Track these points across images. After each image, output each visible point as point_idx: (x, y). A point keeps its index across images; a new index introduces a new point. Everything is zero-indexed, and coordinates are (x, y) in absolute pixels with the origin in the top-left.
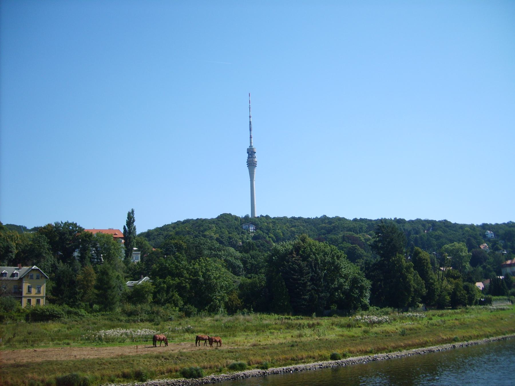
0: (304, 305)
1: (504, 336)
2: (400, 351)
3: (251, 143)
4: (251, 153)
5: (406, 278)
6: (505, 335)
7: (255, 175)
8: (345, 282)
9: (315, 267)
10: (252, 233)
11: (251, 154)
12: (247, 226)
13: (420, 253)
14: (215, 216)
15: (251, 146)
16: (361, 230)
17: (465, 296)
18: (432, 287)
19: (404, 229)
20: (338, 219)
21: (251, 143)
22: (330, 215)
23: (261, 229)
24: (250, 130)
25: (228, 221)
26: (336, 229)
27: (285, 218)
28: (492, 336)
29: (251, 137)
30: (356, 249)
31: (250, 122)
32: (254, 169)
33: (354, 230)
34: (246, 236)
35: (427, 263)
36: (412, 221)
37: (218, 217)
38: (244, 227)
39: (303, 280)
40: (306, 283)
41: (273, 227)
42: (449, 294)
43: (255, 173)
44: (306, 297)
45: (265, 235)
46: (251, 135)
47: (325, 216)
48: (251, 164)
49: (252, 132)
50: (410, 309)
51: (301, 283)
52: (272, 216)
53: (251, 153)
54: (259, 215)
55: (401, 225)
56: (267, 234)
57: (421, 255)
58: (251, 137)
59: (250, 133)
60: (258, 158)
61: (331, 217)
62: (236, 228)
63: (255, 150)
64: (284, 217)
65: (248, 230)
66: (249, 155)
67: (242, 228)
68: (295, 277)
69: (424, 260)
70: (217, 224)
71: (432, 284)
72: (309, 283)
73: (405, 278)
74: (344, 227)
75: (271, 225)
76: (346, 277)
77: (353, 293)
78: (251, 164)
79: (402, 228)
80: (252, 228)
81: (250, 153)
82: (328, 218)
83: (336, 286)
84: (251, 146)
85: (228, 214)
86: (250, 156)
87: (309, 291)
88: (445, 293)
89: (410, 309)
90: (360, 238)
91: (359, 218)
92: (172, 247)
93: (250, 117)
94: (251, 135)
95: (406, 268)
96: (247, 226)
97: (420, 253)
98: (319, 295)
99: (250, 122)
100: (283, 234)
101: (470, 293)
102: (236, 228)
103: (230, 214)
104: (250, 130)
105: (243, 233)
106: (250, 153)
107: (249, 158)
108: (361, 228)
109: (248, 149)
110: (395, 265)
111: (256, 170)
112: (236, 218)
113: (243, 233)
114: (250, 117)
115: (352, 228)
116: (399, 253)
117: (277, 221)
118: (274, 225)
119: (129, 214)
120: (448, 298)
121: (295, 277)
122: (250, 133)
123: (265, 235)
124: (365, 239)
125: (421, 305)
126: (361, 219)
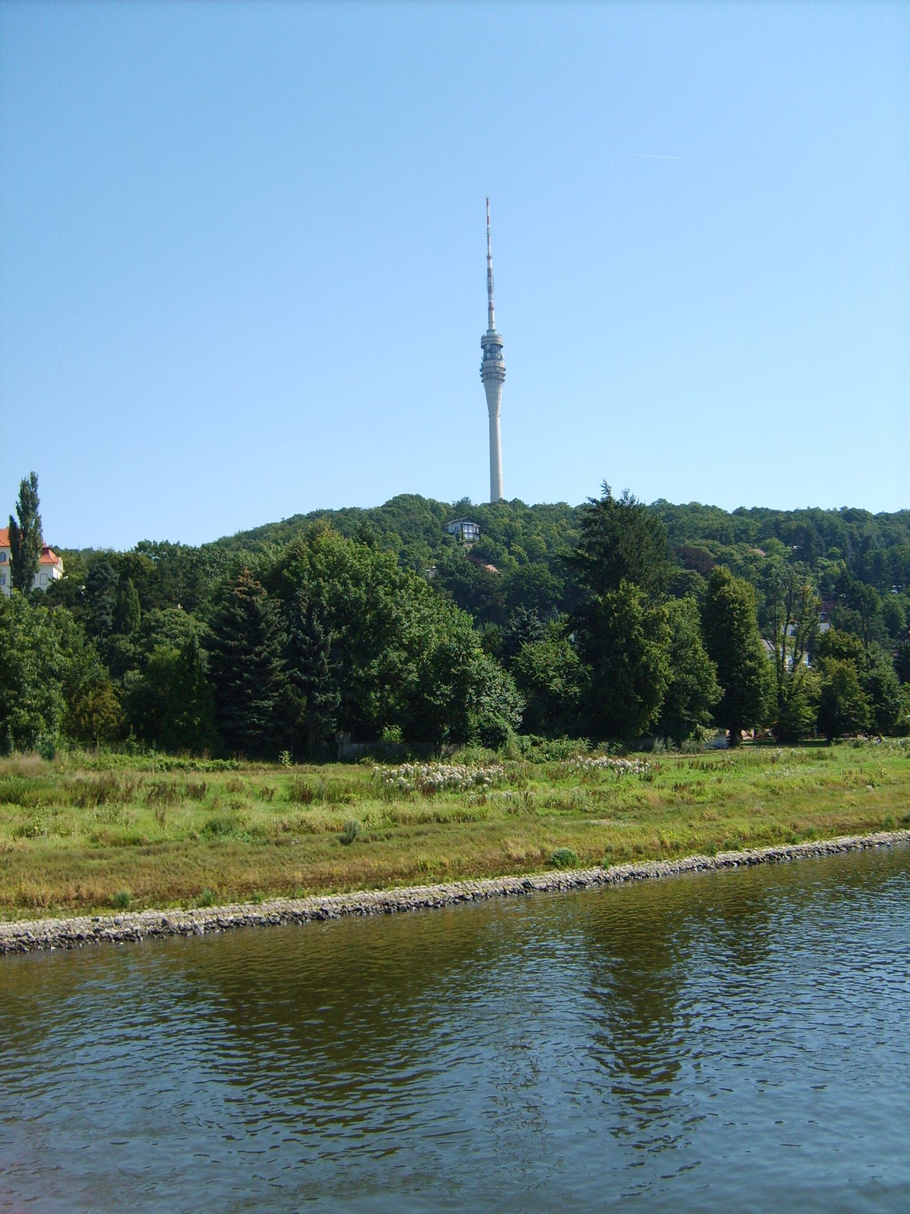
0: (256, 727)
1: (770, 850)
2: (256, 900)
3: (490, 322)
4: (491, 346)
5: (641, 651)
6: (793, 842)
7: (500, 402)
8: (406, 661)
9: (309, 617)
10: (469, 542)
11: (490, 351)
12: (458, 525)
13: (725, 582)
14: (380, 503)
15: (490, 330)
16: (742, 535)
17: (862, 708)
18: (752, 681)
19: (861, 535)
20: (695, 508)
21: (490, 322)
22: (676, 500)
23: (491, 533)
24: (490, 290)
25: (407, 511)
26: (677, 532)
27: (562, 506)
28: (736, 848)
29: (490, 309)
30: (690, 580)
31: (489, 270)
32: (497, 387)
33: (722, 535)
34: (450, 551)
35: (743, 612)
36: (887, 516)
37: (388, 504)
38: (451, 528)
39: (258, 654)
40: (268, 661)
41: (524, 527)
42: (812, 701)
43: (501, 396)
44: (266, 703)
45: (499, 547)
46: (490, 304)
47: (664, 501)
48: (492, 375)
49: (493, 295)
50: (658, 744)
51: (251, 661)
52: (530, 502)
53: (491, 346)
54: (509, 499)
55: (854, 524)
56: (508, 545)
57: (726, 588)
58: (490, 309)
59: (490, 298)
60: (507, 360)
61: (677, 503)
62: (427, 531)
63: (501, 341)
64: (560, 504)
65: (459, 536)
66: (486, 352)
67: (445, 529)
68: (232, 643)
69: (734, 601)
70: (378, 521)
71: (753, 671)
72: (277, 663)
73: (635, 650)
74: (697, 529)
75: (519, 524)
76: (413, 649)
77: (432, 694)
78: (492, 375)
79: (856, 532)
80: (469, 531)
81: (488, 347)
82: (671, 507)
83: (374, 672)
84: (490, 330)
85: (411, 497)
86: (489, 355)
87: (279, 685)
88: (801, 698)
89: (658, 744)
90: (732, 555)
91: (749, 507)
92: (106, 569)
93: (489, 258)
94: (490, 304)
95: (644, 624)
96: (458, 525)
97: (725, 582)
98: (311, 699)
99: (489, 270)
100: (549, 546)
101: (885, 700)
102: (427, 531)
103: (418, 497)
104: (490, 290)
105: (445, 542)
106: (488, 347)
107: (485, 359)
108: (745, 532)
109: (483, 338)
110: (612, 612)
111: (504, 391)
112: (435, 507)
113: (445, 542)
114: (489, 258)
115: (717, 530)
116: (629, 580)
117: (536, 515)
118: (529, 523)
119: (24, 485)
120: (808, 712)
121: (232, 643)
122: (490, 298)
123: (499, 547)
124: (745, 559)
125: (709, 733)
126: (755, 509)
